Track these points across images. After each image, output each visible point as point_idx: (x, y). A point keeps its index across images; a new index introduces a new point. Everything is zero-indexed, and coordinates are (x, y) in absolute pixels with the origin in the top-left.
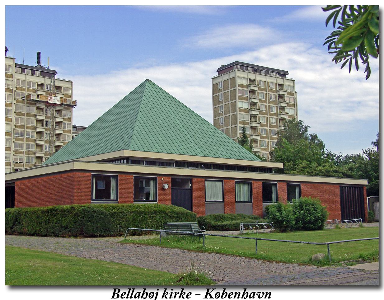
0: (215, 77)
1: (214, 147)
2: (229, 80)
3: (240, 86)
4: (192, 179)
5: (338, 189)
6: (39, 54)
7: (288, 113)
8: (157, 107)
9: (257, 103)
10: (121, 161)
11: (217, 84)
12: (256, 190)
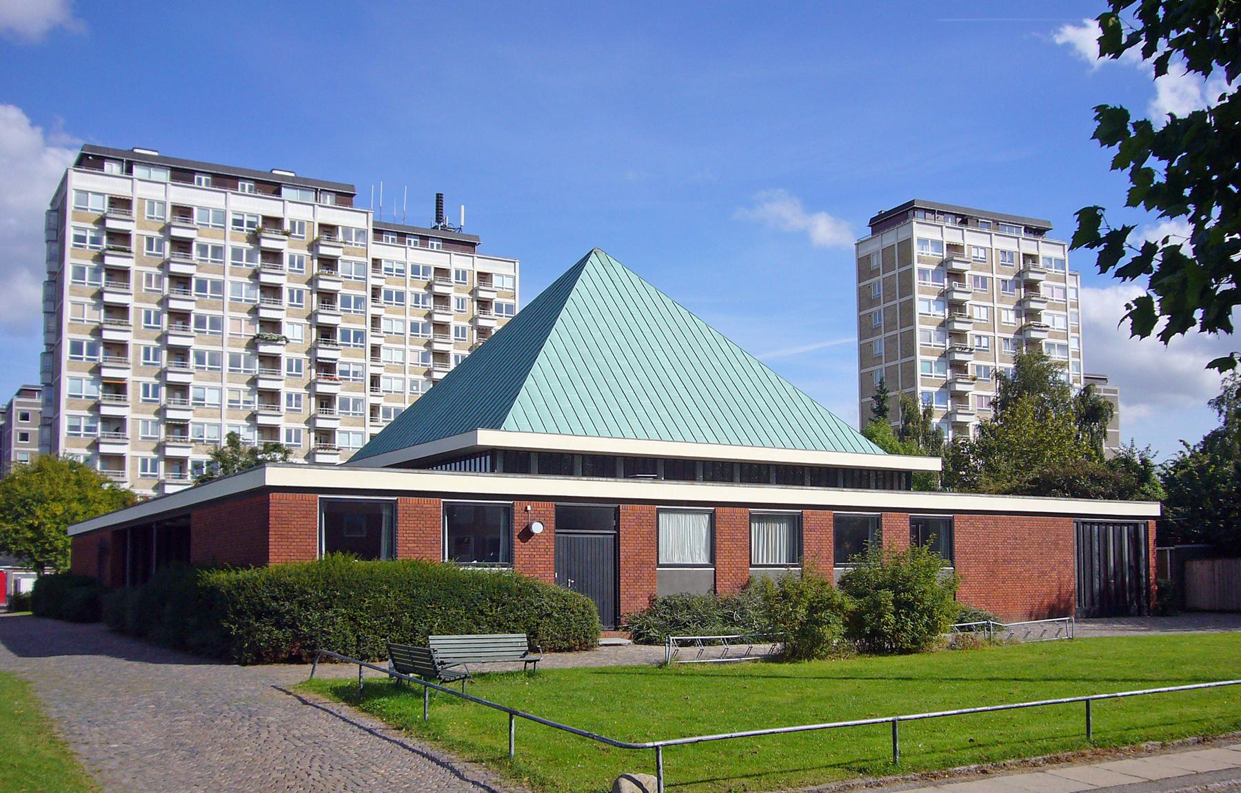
0: (862, 240)
1: (753, 420)
2: (896, 245)
3: (924, 260)
4: (619, 506)
5: (1070, 527)
6: (439, 198)
7: (1047, 326)
8: (609, 318)
9: (968, 303)
10: (446, 467)
11: (868, 257)
12: (813, 535)
